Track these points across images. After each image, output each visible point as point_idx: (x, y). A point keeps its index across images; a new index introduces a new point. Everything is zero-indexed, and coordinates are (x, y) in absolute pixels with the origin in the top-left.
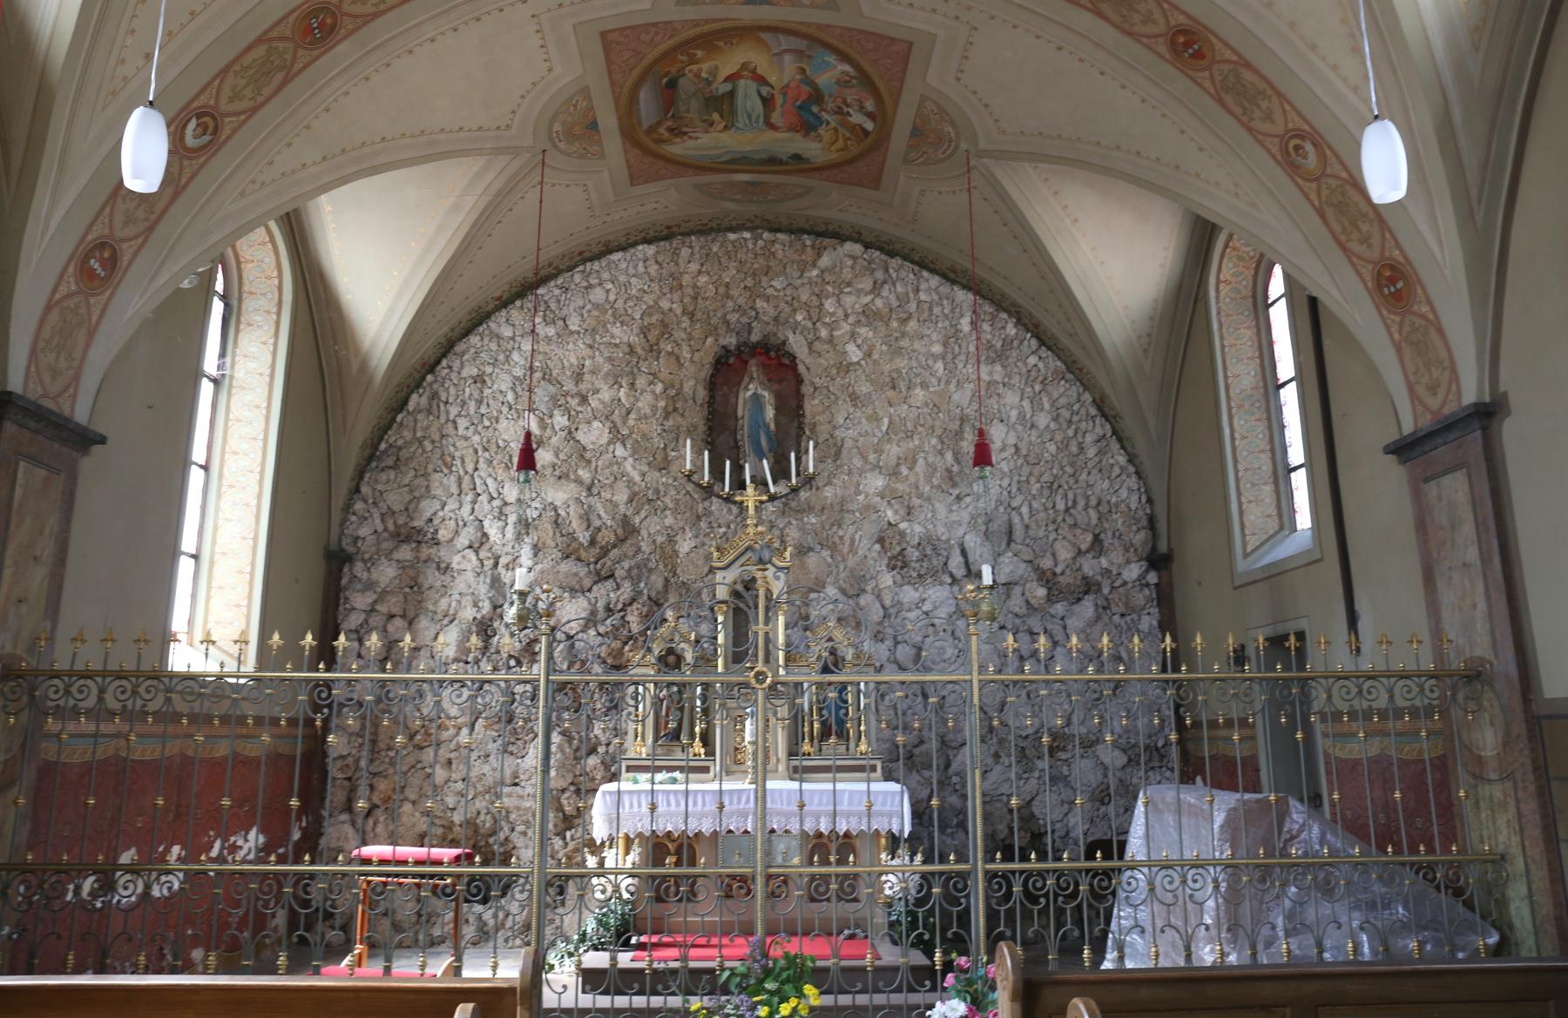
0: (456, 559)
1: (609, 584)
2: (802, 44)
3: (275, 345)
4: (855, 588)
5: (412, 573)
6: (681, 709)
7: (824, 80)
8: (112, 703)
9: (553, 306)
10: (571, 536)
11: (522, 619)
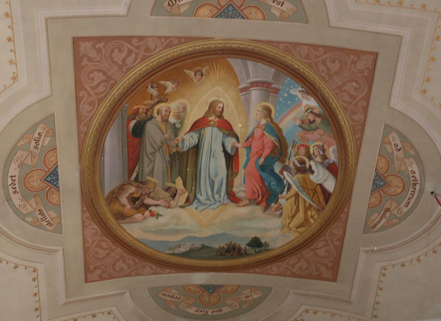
2: (265, 72)
7: (288, 123)
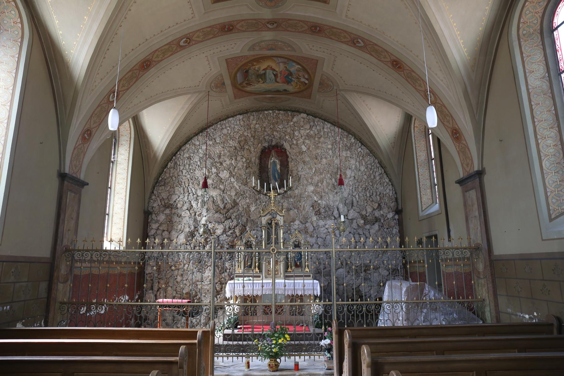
0: (183, 213)
1: (230, 220)
2: (286, 60)
3: (129, 150)
4: (305, 221)
5: (170, 217)
6: (252, 259)
7: (292, 70)
8: (95, 259)
9: (211, 135)
10: (218, 206)
11: (204, 232)
